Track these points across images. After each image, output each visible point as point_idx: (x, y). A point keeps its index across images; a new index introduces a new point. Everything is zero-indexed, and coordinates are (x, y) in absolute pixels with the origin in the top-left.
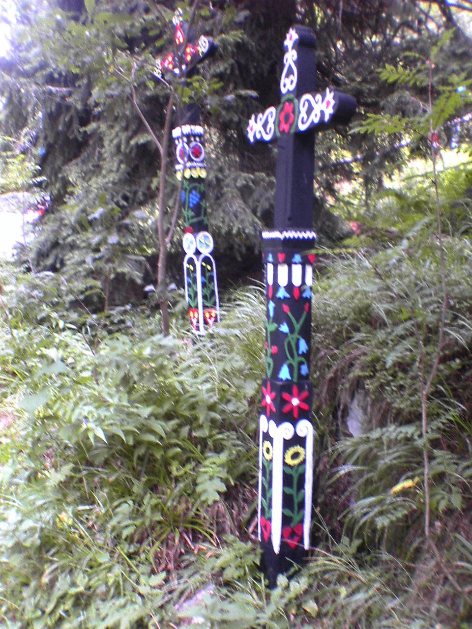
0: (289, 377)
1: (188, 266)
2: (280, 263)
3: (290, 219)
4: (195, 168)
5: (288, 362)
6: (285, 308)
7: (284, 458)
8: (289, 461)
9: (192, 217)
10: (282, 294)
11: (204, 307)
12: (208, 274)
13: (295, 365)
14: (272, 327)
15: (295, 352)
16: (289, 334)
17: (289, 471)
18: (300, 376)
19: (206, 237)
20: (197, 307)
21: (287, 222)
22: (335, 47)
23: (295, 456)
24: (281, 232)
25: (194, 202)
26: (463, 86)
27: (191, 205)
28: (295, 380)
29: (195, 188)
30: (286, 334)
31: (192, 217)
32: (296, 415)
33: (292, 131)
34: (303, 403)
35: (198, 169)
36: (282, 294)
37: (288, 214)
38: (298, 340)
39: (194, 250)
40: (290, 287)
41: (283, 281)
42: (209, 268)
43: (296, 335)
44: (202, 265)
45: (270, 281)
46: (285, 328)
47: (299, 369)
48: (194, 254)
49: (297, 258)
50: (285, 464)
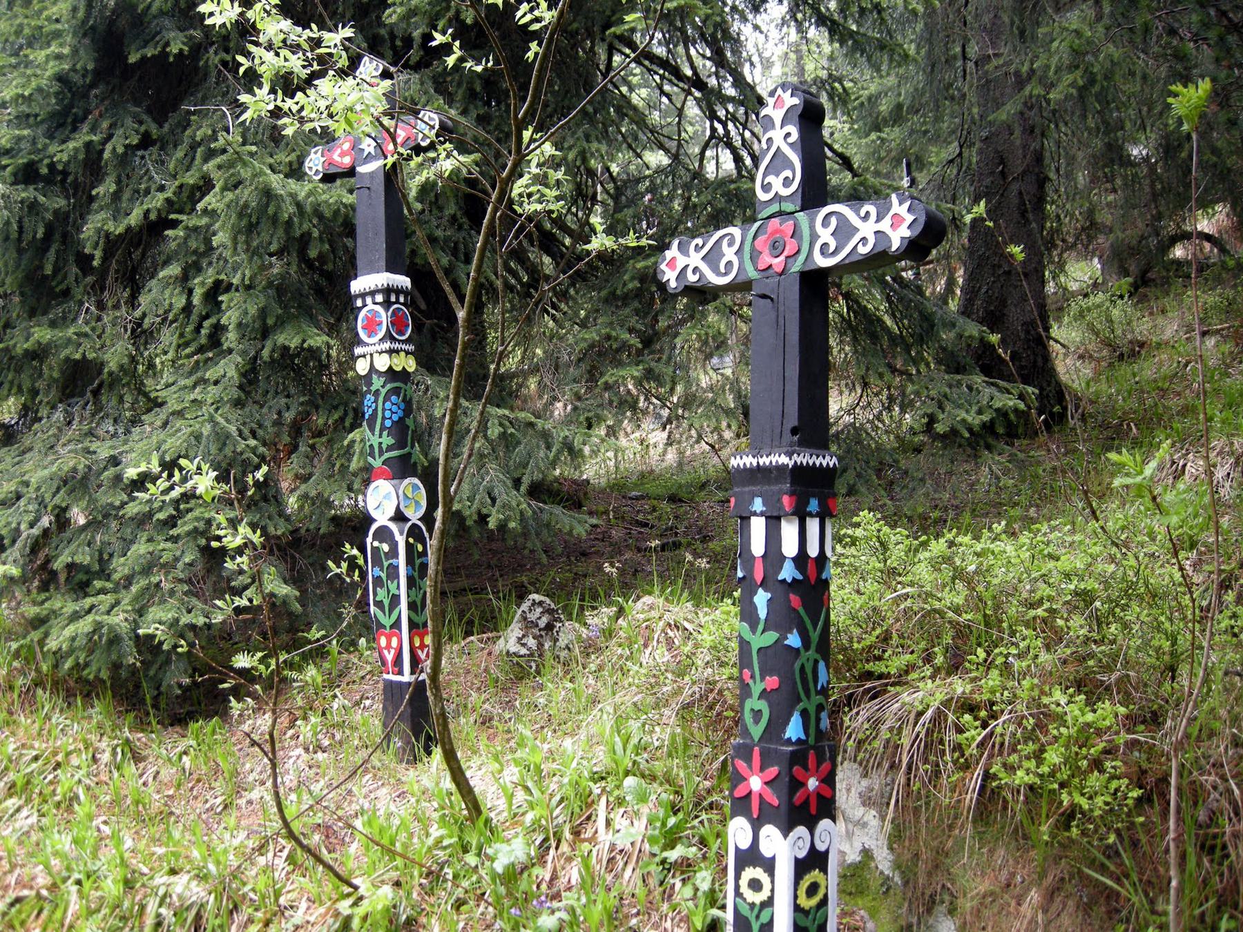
0: (803, 737)
1: (376, 544)
2: (786, 515)
3: (794, 431)
4: (397, 352)
5: (801, 706)
6: (795, 599)
7: (796, 897)
8: (806, 903)
9: (389, 449)
10: (788, 572)
11: (412, 625)
12: (418, 562)
13: (812, 710)
14: (771, 637)
15: (811, 685)
16: (802, 651)
17: (803, 922)
18: (820, 734)
19: (415, 487)
20: (397, 624)
21: (787, 436)
22: (564, 245)
23: (813, 889)
24: (790, 455)
25: (395, 418)
26: (1087, 255)
27: (388, 423)
28: (811, 741)
29: (396, 391)
30: (798, 650)
31: (389, 449)
32: (813, 811)
33: (797, 266)
34: (768, 790)
35: (403, 354)
36: (788, 572)
37: (792, 421)
38: (816, 662)
39: (391, 513)
40: (801, 559)
41: (790, 547)
42: (420, 548)
43: (812, 653)
44: (407, 542)
45: (758, 546)
46: (794, 640)
47: (818, 720)
48: (392, 519)
49: (813, 505)
50: (797, 908)
